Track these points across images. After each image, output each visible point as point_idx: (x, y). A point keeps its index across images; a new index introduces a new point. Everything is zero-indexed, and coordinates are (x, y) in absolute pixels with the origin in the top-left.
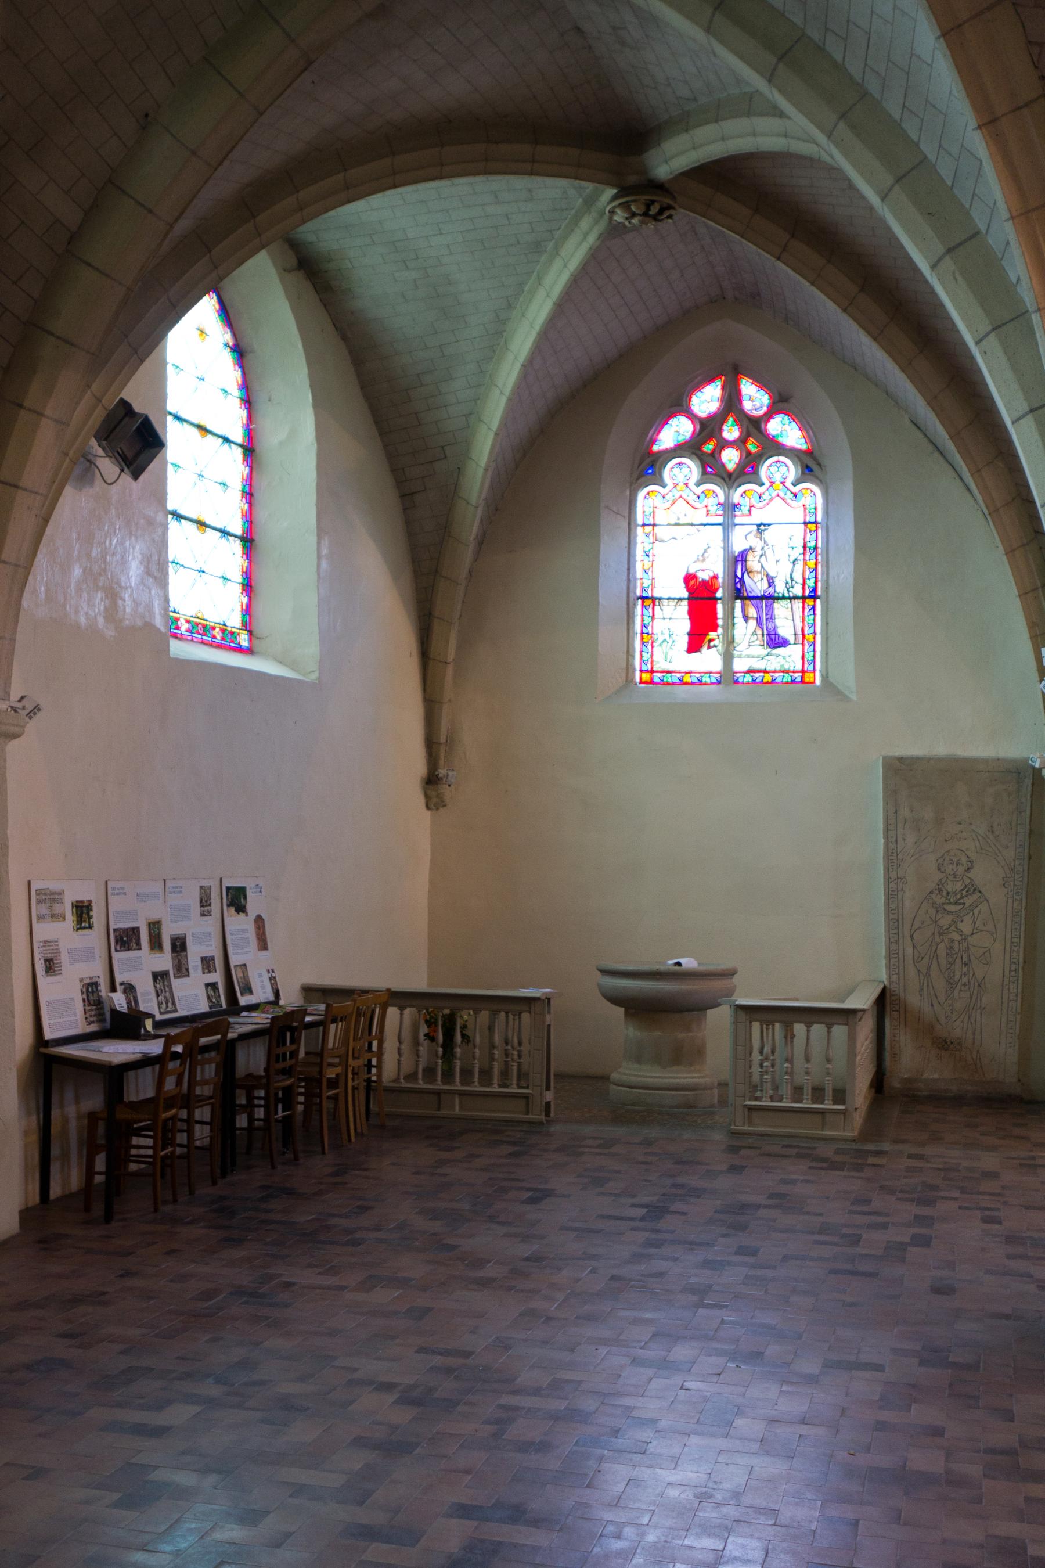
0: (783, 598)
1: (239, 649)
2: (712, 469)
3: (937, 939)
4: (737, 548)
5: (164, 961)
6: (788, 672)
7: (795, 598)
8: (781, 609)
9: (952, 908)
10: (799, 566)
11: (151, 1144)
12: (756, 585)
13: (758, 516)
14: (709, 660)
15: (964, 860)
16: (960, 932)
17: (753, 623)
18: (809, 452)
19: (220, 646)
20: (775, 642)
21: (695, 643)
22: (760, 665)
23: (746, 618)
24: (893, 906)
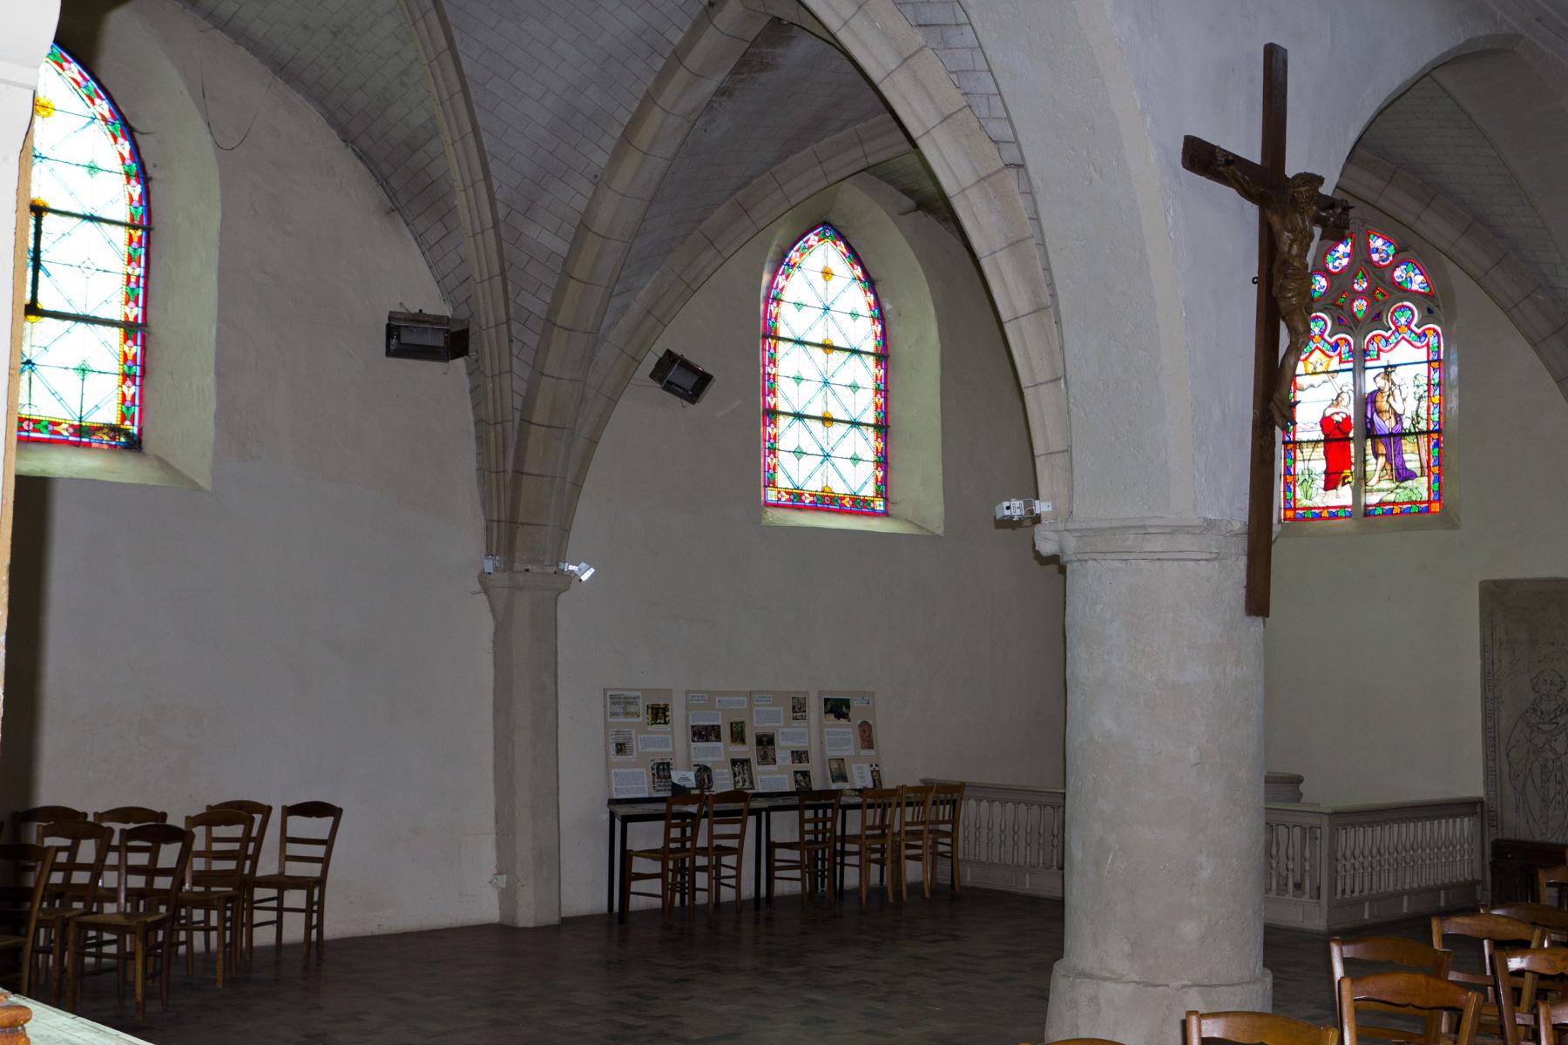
0: (1410, 434)
1: (874, 514)
2: (1345, 320)
3: (1532, 758)
4: (1370, 387)
5: (748, 750)
6: (1415, 502)
7: (1421, 432)
8: (1408, 445)
9: (1548, 727)
10: (1424, 404)
11: (659, 870)
12: (1386, 424)
13: (1385, 359)
14: (1343, 496)
15: (1557, 680)
16: (1554, 751)
17: (1382, 460)
18: (1429, 296)
19: (850, 512)
20: (1403, 475)
21: (1330, 484)
22: (1391, 498)
23: (1376, 455)
24: (1490, 724)
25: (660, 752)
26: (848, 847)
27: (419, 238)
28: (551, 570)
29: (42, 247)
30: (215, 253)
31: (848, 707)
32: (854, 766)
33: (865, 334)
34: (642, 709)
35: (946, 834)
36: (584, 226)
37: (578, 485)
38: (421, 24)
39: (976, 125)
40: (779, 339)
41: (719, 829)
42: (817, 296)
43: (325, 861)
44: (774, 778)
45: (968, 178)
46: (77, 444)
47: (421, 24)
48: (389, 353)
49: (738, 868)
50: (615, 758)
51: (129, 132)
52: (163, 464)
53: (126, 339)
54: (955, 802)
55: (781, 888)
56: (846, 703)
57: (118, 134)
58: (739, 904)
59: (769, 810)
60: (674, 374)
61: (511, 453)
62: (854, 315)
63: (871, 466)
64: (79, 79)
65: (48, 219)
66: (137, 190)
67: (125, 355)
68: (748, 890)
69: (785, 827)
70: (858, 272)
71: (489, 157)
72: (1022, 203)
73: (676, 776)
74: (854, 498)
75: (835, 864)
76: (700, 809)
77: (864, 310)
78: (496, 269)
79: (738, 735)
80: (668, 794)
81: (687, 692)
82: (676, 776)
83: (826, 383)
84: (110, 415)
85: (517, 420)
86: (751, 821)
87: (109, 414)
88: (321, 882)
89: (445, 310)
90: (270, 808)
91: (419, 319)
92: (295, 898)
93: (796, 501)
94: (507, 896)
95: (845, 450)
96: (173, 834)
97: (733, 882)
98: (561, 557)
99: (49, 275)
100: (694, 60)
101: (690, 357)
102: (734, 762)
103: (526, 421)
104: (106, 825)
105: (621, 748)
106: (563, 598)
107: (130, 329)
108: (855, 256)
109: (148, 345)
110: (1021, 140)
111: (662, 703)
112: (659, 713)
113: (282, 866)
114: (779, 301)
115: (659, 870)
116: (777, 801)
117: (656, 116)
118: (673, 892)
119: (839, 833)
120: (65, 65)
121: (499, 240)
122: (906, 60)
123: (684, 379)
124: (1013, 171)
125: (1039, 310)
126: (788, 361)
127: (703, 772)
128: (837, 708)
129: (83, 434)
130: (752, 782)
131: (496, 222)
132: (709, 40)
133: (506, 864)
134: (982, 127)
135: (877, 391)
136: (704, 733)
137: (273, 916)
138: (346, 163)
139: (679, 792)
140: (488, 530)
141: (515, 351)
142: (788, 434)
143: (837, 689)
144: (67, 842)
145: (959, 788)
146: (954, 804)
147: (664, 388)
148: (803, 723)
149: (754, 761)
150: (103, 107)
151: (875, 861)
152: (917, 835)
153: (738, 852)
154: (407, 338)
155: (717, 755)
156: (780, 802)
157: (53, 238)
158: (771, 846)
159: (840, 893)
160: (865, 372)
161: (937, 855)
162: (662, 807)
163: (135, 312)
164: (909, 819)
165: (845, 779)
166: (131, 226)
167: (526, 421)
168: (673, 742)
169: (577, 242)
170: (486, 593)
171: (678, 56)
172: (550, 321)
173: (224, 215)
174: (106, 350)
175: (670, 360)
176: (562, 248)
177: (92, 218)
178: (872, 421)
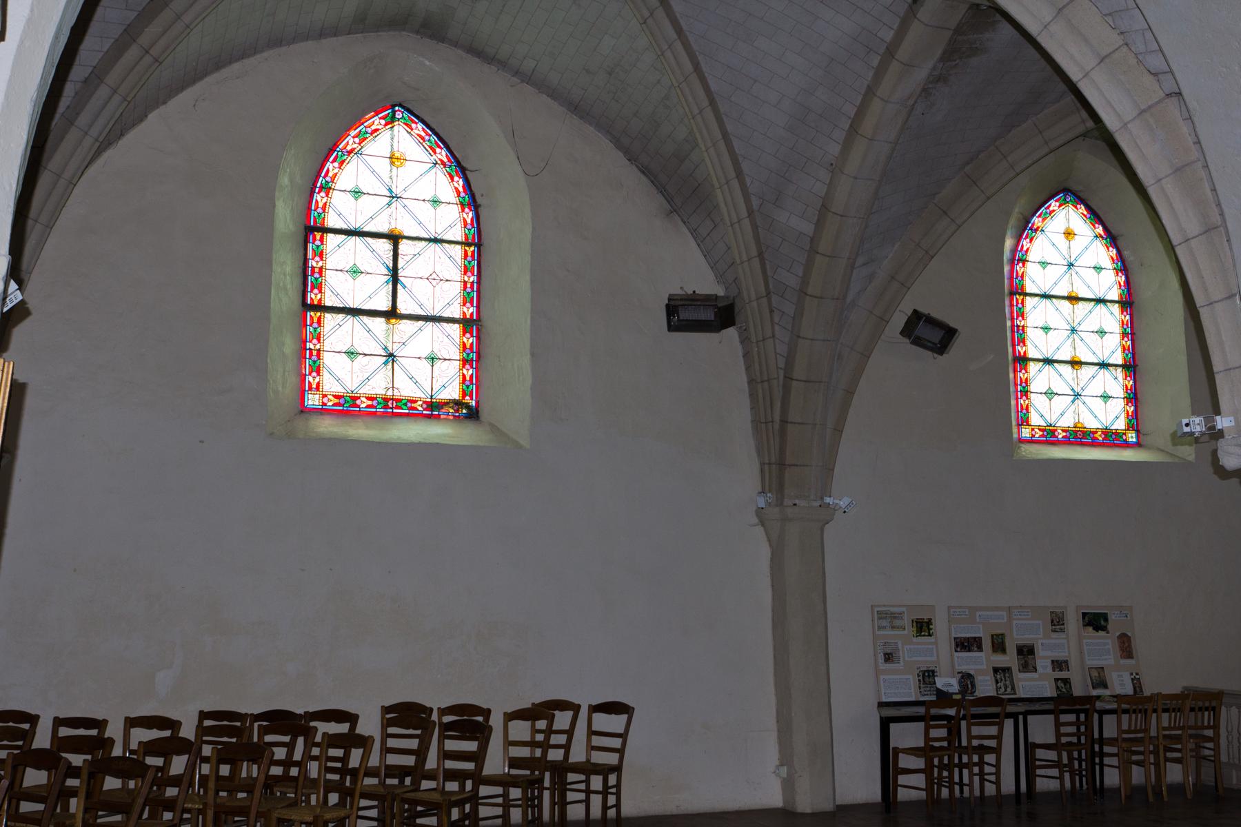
1: (1127, 445)
5: (1009, 659)
11: (923, 766)
19: (1102, 445)
25: (926, 661)
26: (1107, 749)
27: (694, 232)
28: (817, 504)
29: (400, 266)
30: (528, 258)
31: (1106, 620)
32: (1114, 675)
33: (1109, 284)
34: (907, 622)
35: (1210, 739)
36: (824, 208)
37: (839, 430)
38: (668, 54)
39: (1133, 61)
40: (1027, 294)
41: (976, 730)
42: (1080, 255)
43: (621, 751)
44: (1036, 684)
45: (1128, 111)
46: (428, 416)
47: (668, 54)
48: (671, 328)
49: (998, 766)
50: (883, 666)
51: (463, 171)
52: (494, 429)
53: (464, 333)
54: (1214, 709)
55: (1042, 785)
56: (1105, 617)
57: (454, 173)
58: (999, 798)
59: (1026, 714)
60: (922, 330)
61: (778, 405)
62: (1098, 269)
63: (1121, 403)
64: (423, 134)
65: (404, 246)
66: (469, 216)
67: (464, 344)
68: (1008, 786)
69: (1041, 729)
70: (1100, 230)
71: (741, 159)
72: (1185, 129)
73: (940, 683)
74: (1106, 432)
75: (1094, 764)
76: (958, 712)
77: (1107, 263)
78: (754, 252)
79: (999, 645)
80: (934, 698)
81: (949, 608)
82: (940, 683)
83: (1073, 330)
84: (453, 392)
85: (781, 377)
86: (1009, 724)
87: (453, 392)
88: (617, 769)
89: (720, 291)
90: (579, 706)
91: (694, 300)
92: (596, 782)
93: (1049, 436)
94: (788, 785)
95: (1096, 388)
96: (183, 746)
97: (993, 778)
98: (826, 490)
99: (404, 287)
100: (903, 53)
101: (935, 314)
102: (996, 670)
103: (788, 378)
104: (313, 724)
105: (888, 658)
106: (829, 531)
107: (466, 324)
108: (1095, 216)
109: (482, 336)
110: (1174, 68)
111: (926, 617)
112: (923, 627)
113: (588, 755)
114: (1024, 262)
115: (923, 766)
116: (1036, 705)
117: (876, 105)
118: (940, 786)
119: (1096, 736)
120: (414, 126)
121: (755, 227)
122: (1060, 10)
123: (929, 333)
124: (1174, 100)
125: (1209, 230)
126: (1036, 314)
127: (967, 680)
128: (1096, 621)
129: (434, 409)
130: (1013, 688)
131: (750, 213)
132: (916, 31)
133: (786, 758)
134: (1140, 62)
135: (1124, 335)
136: (966, 644)
137: (582, 796)
138: (631, 177)
139: (943, 698)
140: (762, 471)
141: (776, 319)
142: (1039, 378)
143: (1095, 603)
144: (287, 739)
145: (1219, 696)
146: (1215, 710)
147: (914, 343)
148: (1063, 635)
149: (1015, 669)
150: (442, 154)
151: (1138, 763)
152: (1177, 739)
153: (997, 751)
154: (686, 315)
155: (980, 663)
156: (1037, 707)
157: (407, 258)
158: (1031, 748)
159: (1101, 791)
160: (1112, 319)
161: (1200, 758)
162: (921, 710)
163: (470, 310)
164: (1166, 724)
165: (1105, 686)
166: (466, 243)
167: (788, 378)
168: (938, 653)
169: (820, 224)
170: (763, 525)
171: (890, 52)
172: (802, 292)
173: (534, 229)
174: (448, 342)
175: (917, 317)
176: (808, 228)
177: (436, 241)
178: (1120, 362)
